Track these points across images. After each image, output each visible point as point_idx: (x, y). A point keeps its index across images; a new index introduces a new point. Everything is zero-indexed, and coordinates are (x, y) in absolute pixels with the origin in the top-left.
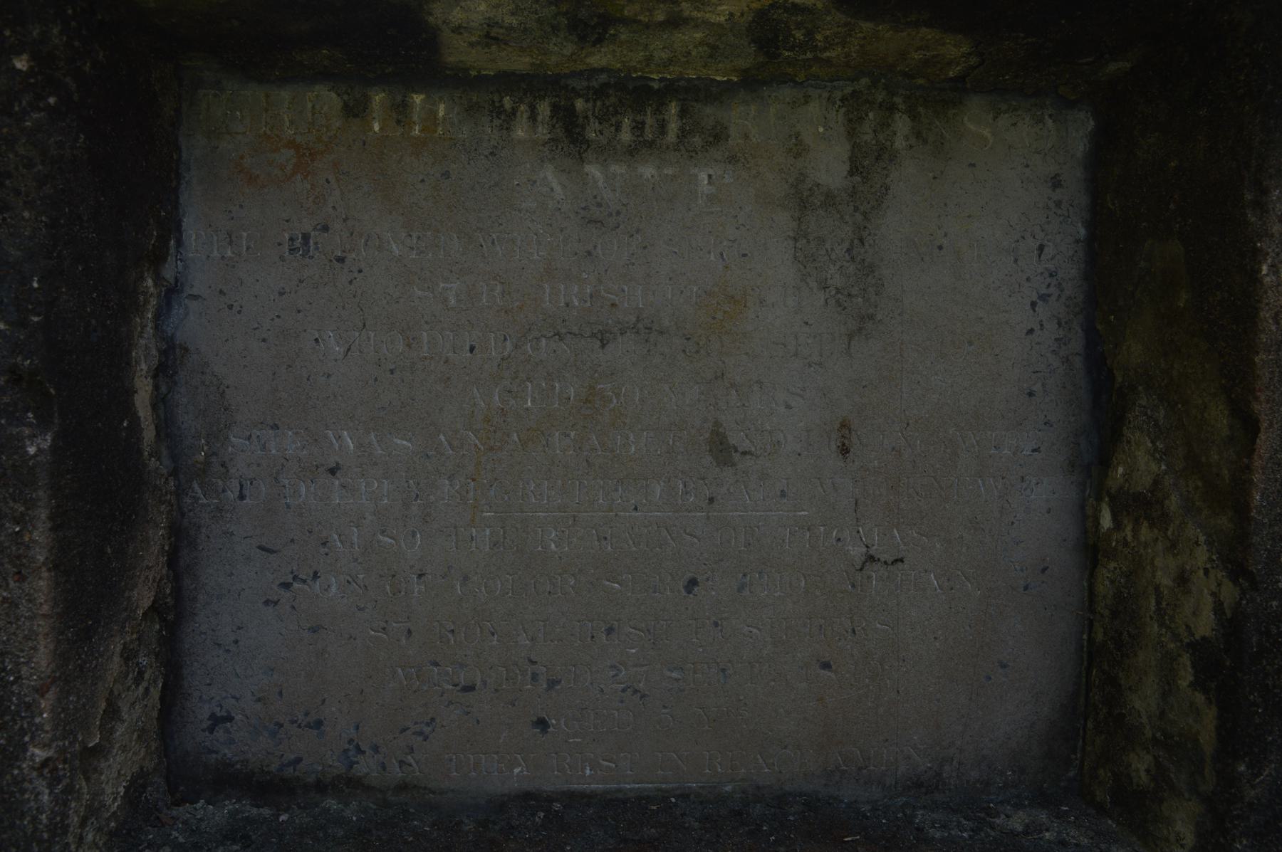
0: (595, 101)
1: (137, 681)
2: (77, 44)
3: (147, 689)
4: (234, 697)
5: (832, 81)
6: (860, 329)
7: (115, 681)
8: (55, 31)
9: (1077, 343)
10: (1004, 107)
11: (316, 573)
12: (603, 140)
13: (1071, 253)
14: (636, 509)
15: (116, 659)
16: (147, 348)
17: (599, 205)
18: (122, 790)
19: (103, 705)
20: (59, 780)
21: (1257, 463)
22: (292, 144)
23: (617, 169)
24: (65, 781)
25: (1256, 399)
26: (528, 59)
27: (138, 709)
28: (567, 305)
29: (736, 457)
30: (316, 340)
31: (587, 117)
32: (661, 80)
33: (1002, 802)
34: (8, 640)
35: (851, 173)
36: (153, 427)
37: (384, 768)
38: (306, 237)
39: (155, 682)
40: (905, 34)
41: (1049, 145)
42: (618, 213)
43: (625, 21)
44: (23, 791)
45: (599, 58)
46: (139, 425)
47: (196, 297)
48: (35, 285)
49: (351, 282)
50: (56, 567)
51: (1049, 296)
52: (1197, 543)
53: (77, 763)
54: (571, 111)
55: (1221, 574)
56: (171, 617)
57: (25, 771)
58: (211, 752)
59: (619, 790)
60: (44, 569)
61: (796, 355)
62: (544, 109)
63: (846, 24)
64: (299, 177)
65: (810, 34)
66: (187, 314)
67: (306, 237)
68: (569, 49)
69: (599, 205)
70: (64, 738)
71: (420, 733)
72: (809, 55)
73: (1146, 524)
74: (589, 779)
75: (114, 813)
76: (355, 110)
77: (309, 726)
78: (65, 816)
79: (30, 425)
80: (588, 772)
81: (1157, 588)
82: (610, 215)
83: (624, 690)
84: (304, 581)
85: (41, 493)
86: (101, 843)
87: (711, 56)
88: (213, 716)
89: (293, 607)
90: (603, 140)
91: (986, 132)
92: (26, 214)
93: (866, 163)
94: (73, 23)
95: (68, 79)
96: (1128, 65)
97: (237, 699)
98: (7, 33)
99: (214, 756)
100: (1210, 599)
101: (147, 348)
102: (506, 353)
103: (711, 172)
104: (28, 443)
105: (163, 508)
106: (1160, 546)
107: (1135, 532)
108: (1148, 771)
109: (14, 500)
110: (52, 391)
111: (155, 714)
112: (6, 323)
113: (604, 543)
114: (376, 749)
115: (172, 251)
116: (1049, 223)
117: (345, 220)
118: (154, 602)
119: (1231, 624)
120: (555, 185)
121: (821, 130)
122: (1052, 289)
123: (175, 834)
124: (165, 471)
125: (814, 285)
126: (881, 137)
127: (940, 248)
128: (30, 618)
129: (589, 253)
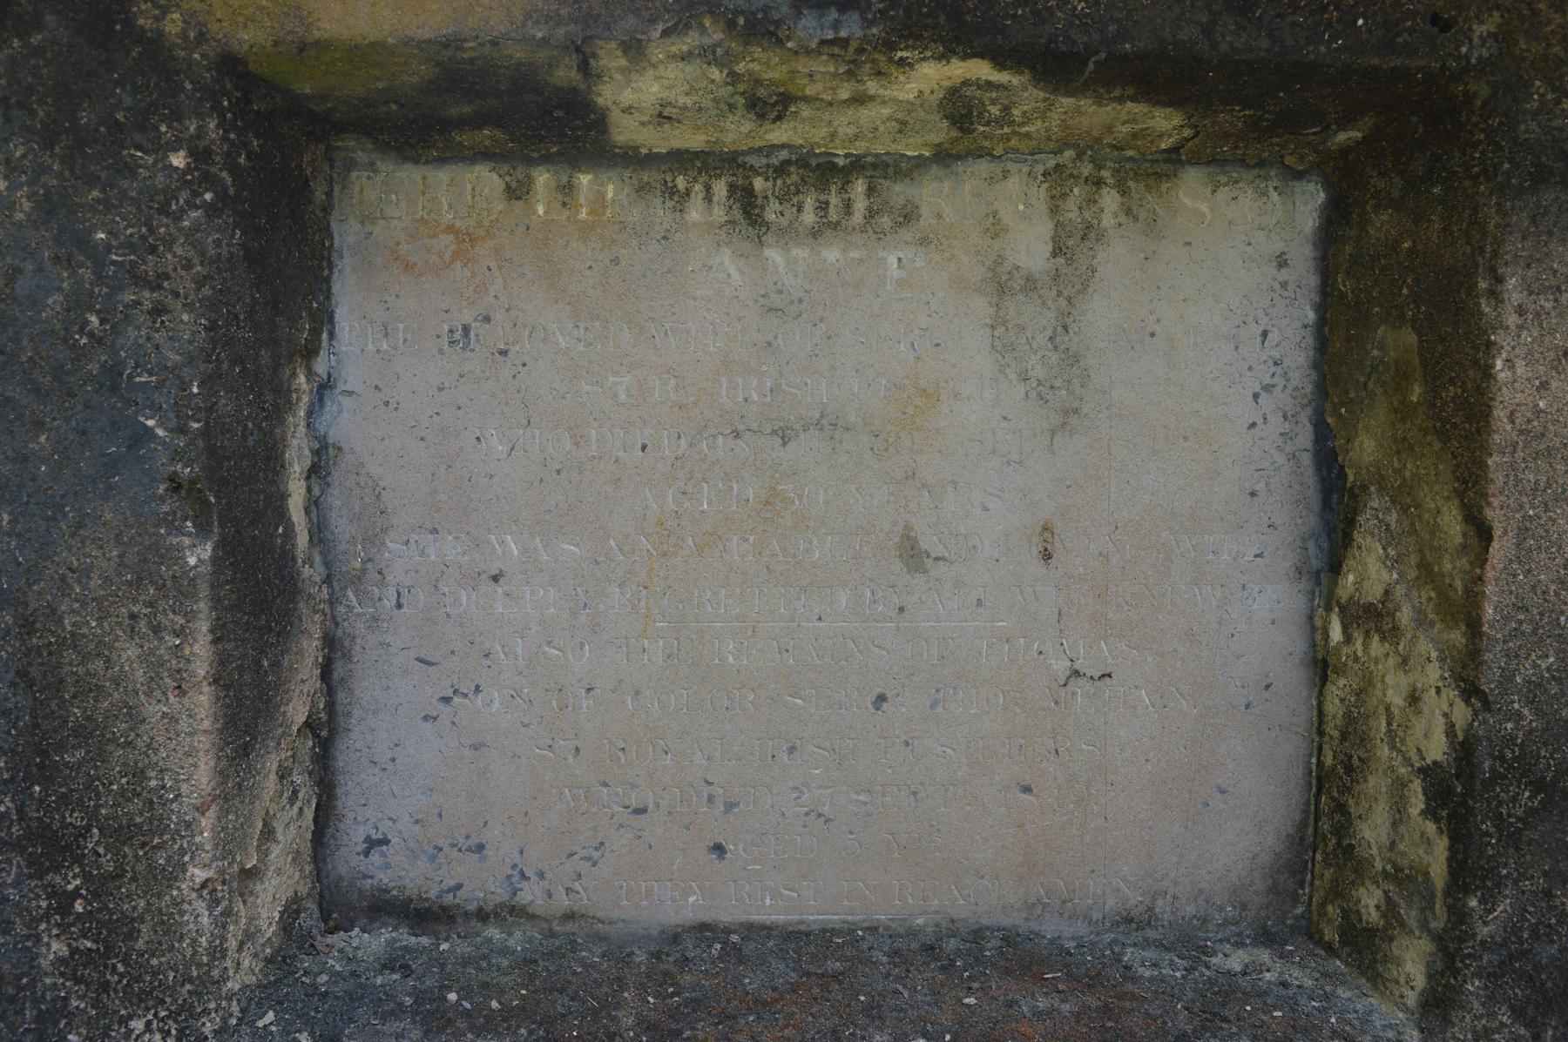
0: (774, 179)
2: (232, 136)
3: (301, 809)
6: (1064, 424)
8: (212, 125)
10: (1224, 179)
11: (477, 687)
12: (784, 222)
13: (1299, 338)
15: (273, 777)
16: (300, 448)
17: (780, 292)
18: (277, 915)
20: (217, 902)
21: (1490, 574)
22: (450, 229)
23: (800, 253)
24: (224, 903)
25: (1489, 504)
26: (703, 138)
27: (293, 829)
29: (929, 563)
32: (847, 156)
33: (1221, 941)
35: (1054, 254)
37: (550, 896)
38: (466, 329)
43: (806, 99)
44: (182, 913)
45: (778, 134)
47: (350, 393)
48: (195, 390)
54: (749, 192)
55: (1453, 693)
56: (324, 733)
58: (366, 877)
59: (802, 922)
61: (994, 452)
62: (720, 188)
63: (1045, 100)
65: (1006, 109)
66: (340, 411)
67: (466, 329)
68: (747, 126)
69: (780, 292)
71: (589, 859)
72: (1006, 130)
73: (1376, 637)
74: (770, 909)
76: (517, 192)
78: (224, 939)
79: (189, 535)
80: (768, 902)
81: (1388, 709)
82: (792, 302)
83: (807, 814)
84: (465, 695)
85: (202, 605)
86: (257, 970)
87: (900, 132)
88: (368, 839)
90: (784, 222)
91: (1204, 208)
92: (185, 317)
93: (1071, 243)
95: (224, 174)
96: (1359, 135)
98: (163, 129)
100: (1442, 720)
103: (901, 255)
105: (317, 617)
106: (1391, 662)
107: (1366, 645)
108: (1377, 907)
109: (174, 612)
110: (212, 499)
111: (309, 836)
113: (785, 655)
114: (541, 875)
115: (325, 344)
116: (1273, 306)
118: (309, 717)
119: (1464, 749)
120: (732, 269)
121: (1021, 207)
122: (1276, 380)
123: (331, 962)
124: (318, 579)
125: (1013, 376)
126: (1087, 215)
127: (1152, 335)
128: (191, 734)
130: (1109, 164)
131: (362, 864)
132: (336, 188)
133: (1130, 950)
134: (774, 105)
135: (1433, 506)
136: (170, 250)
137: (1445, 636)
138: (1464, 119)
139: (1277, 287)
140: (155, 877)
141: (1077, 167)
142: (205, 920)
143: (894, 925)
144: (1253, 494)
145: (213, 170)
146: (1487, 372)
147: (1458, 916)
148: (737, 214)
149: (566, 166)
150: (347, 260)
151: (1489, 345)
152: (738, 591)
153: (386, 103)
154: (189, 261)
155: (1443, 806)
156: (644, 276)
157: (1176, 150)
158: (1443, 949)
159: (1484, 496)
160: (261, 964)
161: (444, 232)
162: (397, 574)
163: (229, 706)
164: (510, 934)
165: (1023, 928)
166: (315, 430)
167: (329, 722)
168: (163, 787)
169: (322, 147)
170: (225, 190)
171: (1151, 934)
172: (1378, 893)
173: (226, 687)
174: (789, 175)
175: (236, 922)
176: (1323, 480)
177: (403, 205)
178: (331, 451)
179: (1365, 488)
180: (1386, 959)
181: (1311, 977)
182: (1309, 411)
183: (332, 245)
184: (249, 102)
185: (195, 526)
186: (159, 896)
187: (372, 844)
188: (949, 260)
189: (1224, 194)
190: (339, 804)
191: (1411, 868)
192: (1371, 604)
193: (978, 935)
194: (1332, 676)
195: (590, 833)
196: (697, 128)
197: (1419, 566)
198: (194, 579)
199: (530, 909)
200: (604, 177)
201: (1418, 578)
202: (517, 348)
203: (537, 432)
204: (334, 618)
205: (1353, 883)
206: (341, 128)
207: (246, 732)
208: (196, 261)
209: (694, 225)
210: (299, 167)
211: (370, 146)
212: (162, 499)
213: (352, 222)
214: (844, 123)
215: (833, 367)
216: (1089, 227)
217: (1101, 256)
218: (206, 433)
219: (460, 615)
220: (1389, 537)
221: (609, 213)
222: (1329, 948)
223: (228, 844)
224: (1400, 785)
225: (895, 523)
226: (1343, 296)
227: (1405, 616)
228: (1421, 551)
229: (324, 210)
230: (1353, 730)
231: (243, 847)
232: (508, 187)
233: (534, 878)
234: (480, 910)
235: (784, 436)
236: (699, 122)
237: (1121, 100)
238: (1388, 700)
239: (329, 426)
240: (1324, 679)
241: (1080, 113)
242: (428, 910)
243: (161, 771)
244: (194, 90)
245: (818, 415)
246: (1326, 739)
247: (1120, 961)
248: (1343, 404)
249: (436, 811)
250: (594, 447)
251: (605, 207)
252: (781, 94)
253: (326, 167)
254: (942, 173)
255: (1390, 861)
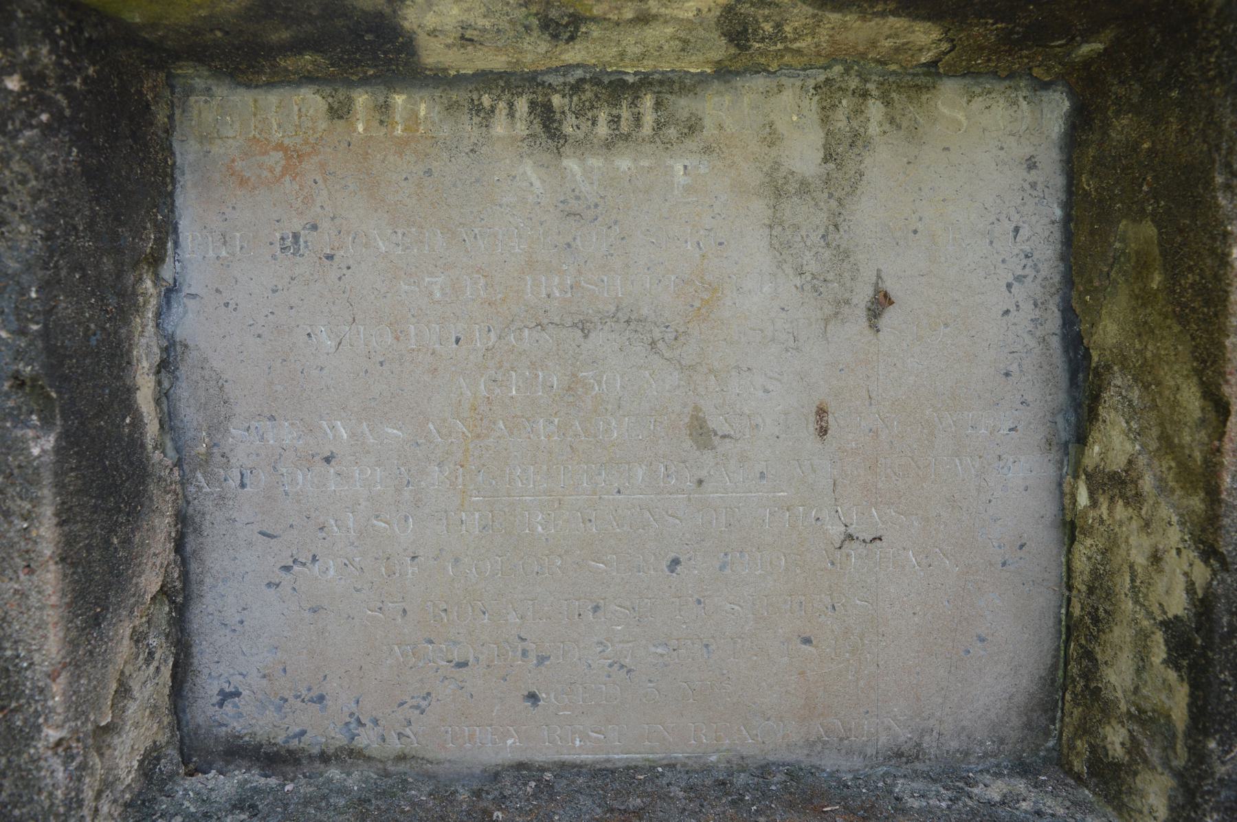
0: (571, 96)
1: (148, 661)
2: (66, 61)
3: (158, 668)
4: (241, 674)
5: (804, 70)
7: (126, 663)
9: (1054, 321)
10: (978, 90)
11: (314, 556)
13: (1047, 233)
14: (619, 492)
15: (126, 642)
16: (148, 346)
17: (578, 198)
18: (136, 764)
19: (114, 686)
20: (73, 758)
23: (595, 162)
24: (79, 759)
25: (1227, 382)
26: (504, 58)
27: (151, 686)
28: (549, 296)
29: (716, 440)
30: (309, 335)
31: (563, 112)
32: (636, 74)
33: (981, 771)
34: (21, 629)
36: (156, 422)
37: (384, 740)
38: (296, 236)
39: (165, 661)
40: (873, 23)
41: (1024, 127)
42: (596, 206)
43: (594, 19)
44: (39, 769)
45: (573, 54)
46: (142, 420)
47: (194, 296)
48: (34, 295)
49: (340, 279)
50: (63, 560)
51: (1025, 277)
52: (1169, 523)
53: (90, 741)
54: (548, 107)
56: (179, 599)
57: (41, 750)
58: (221, 725)
59: (608, 761)
60: (51, 562)
61: (773, 340)
62: (522, 105)
63: (814, 16)
64: (288, 178)
65: (778, 26)
66: (186, 312)
67: (296, 236)
68: (543, 47)
69: (578, 198)
70: (77, 719)
71: (417, 707)
72: (780, 46)
73: (1121, 502)
74: (580, 746)
75: (129, 785)
76: (339, 112)
77: (311, 700)
78: (79, 791)
79: (35, 427)
80: (578, 743)
81: (1131, 567)
82: (589, 207)
83: (611, 666)
84: (304, 564)
85: (46, 491)
87: (683, 50)
88: (221, 692)
89: (294, 589)
91: (960, 116)
92: (23, 228)
94: (62, 43)
95: (59, 97)
96: (1101, 47)
97: (244, 676)
99: (224, 728)
100: (1182, 579)
101: (148, 346)
102: (490, 344)
104: (32, 444)
106: (1135, 525)
107: (1111, 510)
108: (1123, 744)
109: (21, 498)
110: (54, 395)
111: (167, 691)
112: (9, 331)
113: (589, 525)
114: (376, 722)
115: (170, 252)
116: (1024, 204)
117: (333, 219)
118: (162, 587)
119: (1204, 605)
120: (534, 179)
121: (795, 118)
122: (1027, 271)
125: (790, 271)
126: (855, 124)
127: (915, 232)
129: (569, 245)
130: (874, 78)
131: (218, 713)
132: (178, 112)
133: (900, 781)
134: (566, 26)
135: (1172, 383)
136: (8, 166)
137: (1185, 502)
138: (1199, 26)
139: (1027, 186)
140: (14, 737)
141: (849, 79)
142: (60, 775)
143: (690, 763)
144: (1007, 374)
145: (49, 92)
146: (1224, 260)
147: (1199, 756)
148: (538, 128)
149: (382, 88)
150: (188, 176)
151: (1226, 235)
152: (545, 467)
153: (212, 30)
154: (24, 176)
155: (1184, 656)
156: (455, 185)
157: (934, 63)
158: (1183, 784)
159: (1222, 374)
160: (120, 809)
161: (276, 149)
162: (240, 457)
163: (77, 582)
164: (349, 774)
165: (806, 763)
166: (164, 329)
167: (183, 589)
168: (18, 656)
169: (162, 75)
170: (61, 111)
171: (918, 766)
172: (1123, 732)
173: (73, 564)
174: (584, 92)
175: (92, 775)
176: (1070, 361)
177: (237, 126)
178: (178, 348)
179: (1108, 368)
180: (1130, 791)
181: (1063, 806)
182: (1057, 298)
183: (174, 163)
184: (81, 32)
185: (40, 419)
186: (19, 753)
187: (226, 696)
188: (730, 166)
189: (978, 103)
190: (195, 661)
191: (1154, 711)
192: (1115, 473)
193: (765, 770)
194: (1079, 537)
195: (418, 685)
196: (498, 49)
197: (1159, 438)
198: (37, 468)
199: (367, 753)
200: (417, 97)
201: (1158, 449)
202: (342, 253)
203: (362, 328)
204: (185, 496)
205: (1100, 721)
206: (176, 56)
207: (97, 604)
208: (31, 176)
209: (499, 138)
210: (140, 93)
211: (206, 73)
212: (7, 395)
213: (192, 142)
214: (631, 42)
215: (627, 266)
216: (857, 135)
217: (868, 161)
218: (45, 334)
219: (297, 493)
220: (1132, 412)
221: (422, 129)
222: (1078, 778)
223: (78, 706)
224: (1143, 637)
225: (685, 405)
226: (1087, 194)
227: (1147, 484)
228: (1161, 424)
229: (167, 131)
230: (1099, 584)
231: (96, 706)
232: (331, 108)
233: (369, 725)
234: (323, 753)
235: (584, 328)
236: (499, 44)
237: (883, 14)
238: (1131, 559)
239: (176, 326)
240: (1073, 539)
241: (846, 29)
242: (277, 753)
243: (16, 642)
244: (26, 18)
245: (614, 309)
246: (1075, 592)
247: (891, 792)
248: (1088, 292)
249: (281, 667)
250: (413, 341)
251: (418, 124)
252: (571, 15)
253: (167, 93)
254: (722, 88)
255: (1134, 703)
